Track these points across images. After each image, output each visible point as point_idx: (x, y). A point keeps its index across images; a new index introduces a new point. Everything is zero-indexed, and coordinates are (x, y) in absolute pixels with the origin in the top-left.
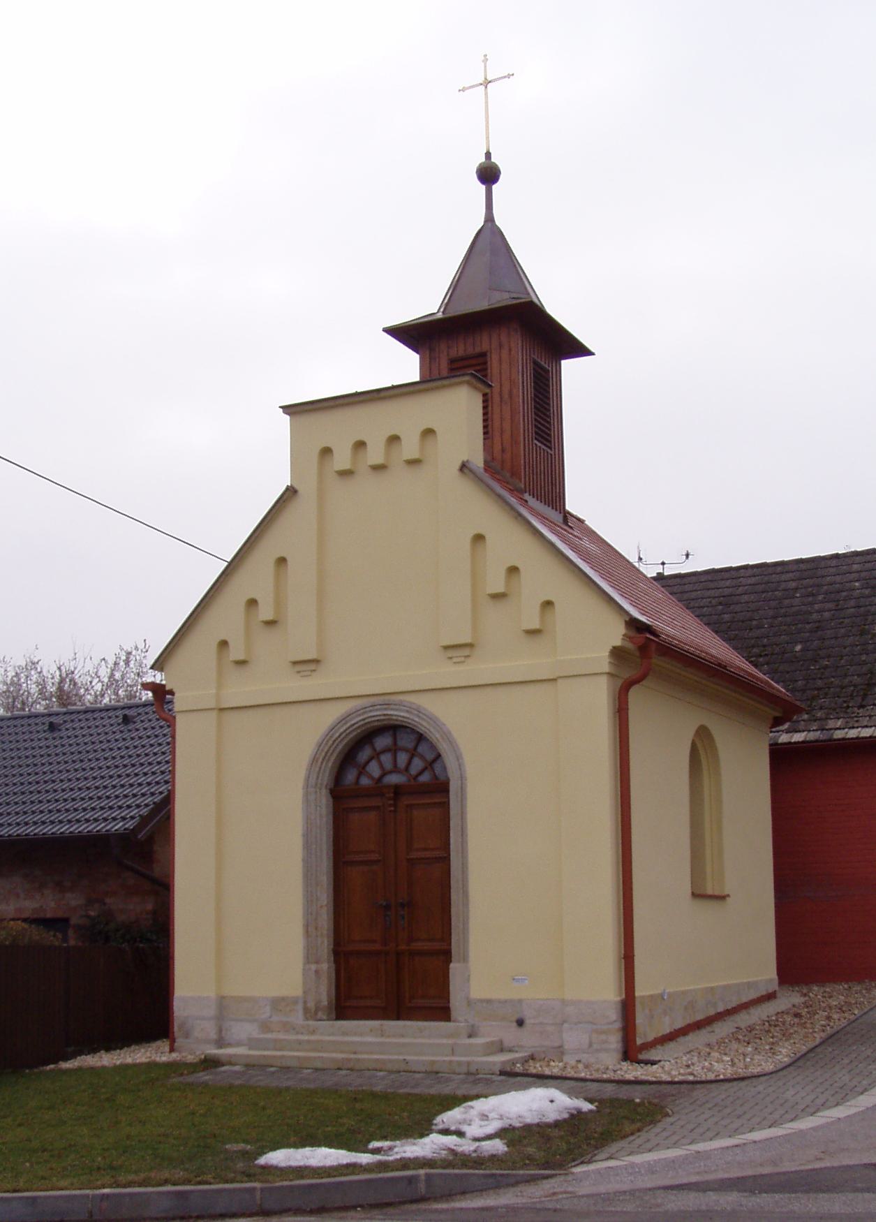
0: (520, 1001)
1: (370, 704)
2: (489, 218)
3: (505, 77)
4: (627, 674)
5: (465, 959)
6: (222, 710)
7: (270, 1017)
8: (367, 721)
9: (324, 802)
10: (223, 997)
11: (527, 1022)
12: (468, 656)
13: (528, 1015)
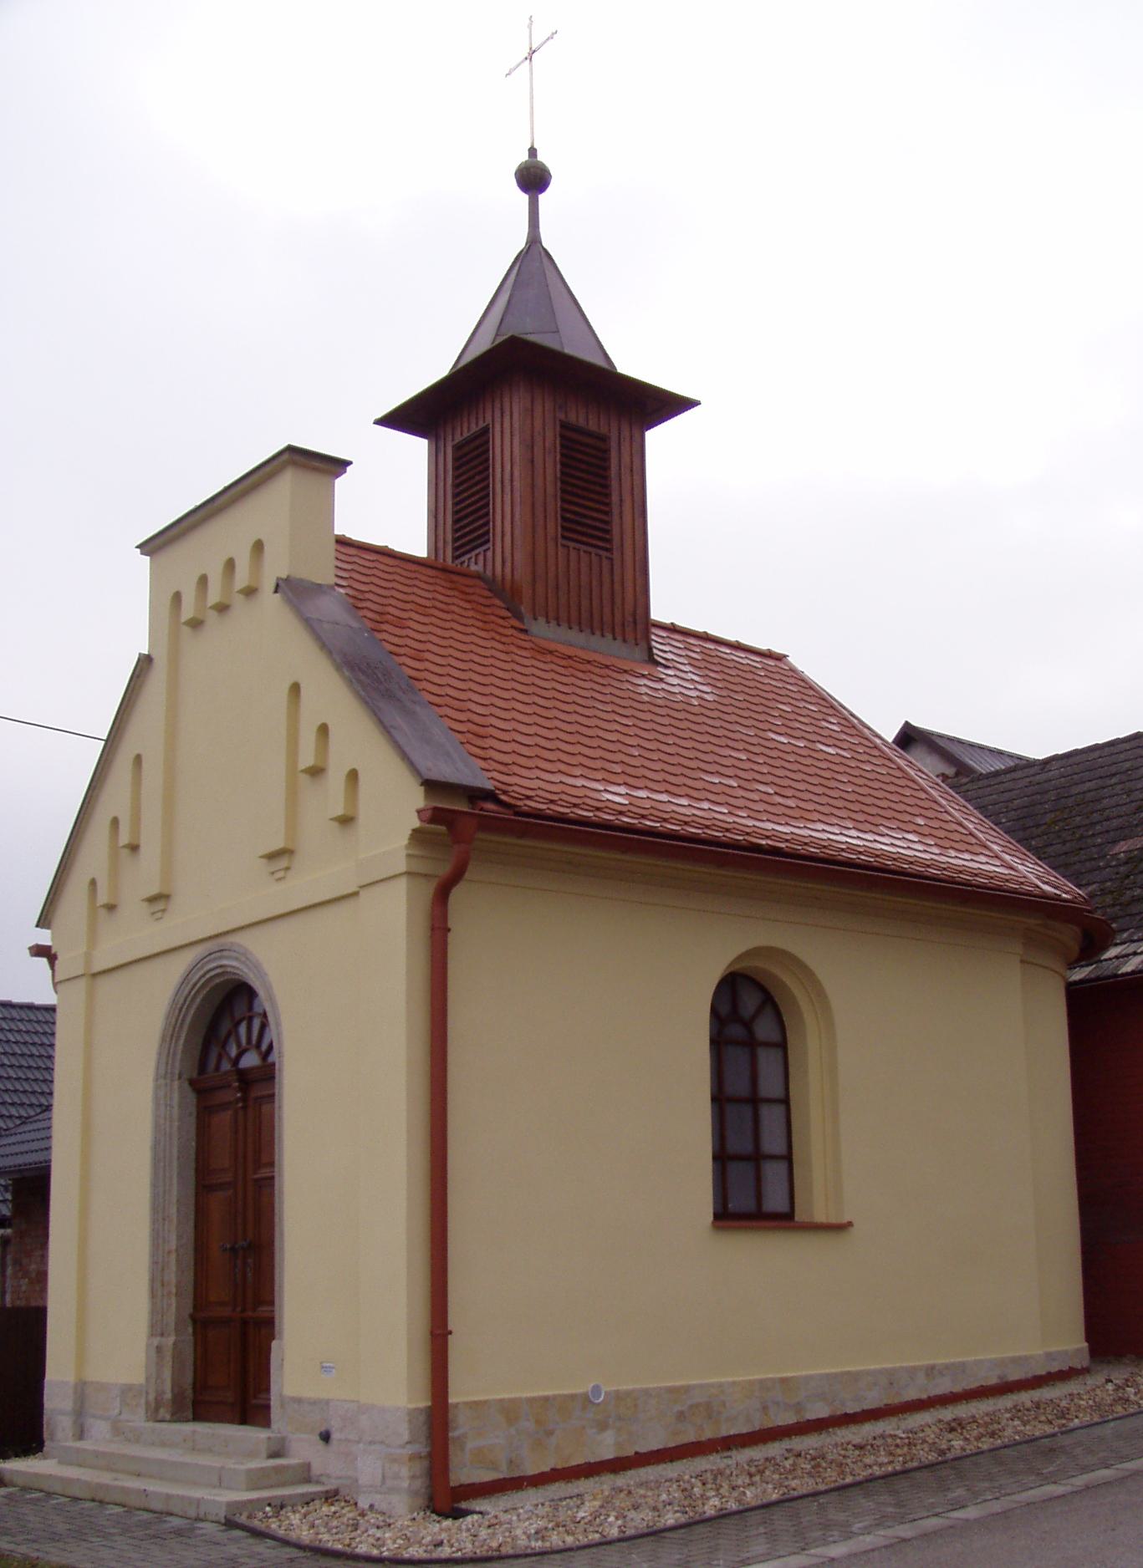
0: (327, 1402)
1: (207, 953)
2: (534, 239)
3: (548, 39)
4: (444, 869)
5: (281, 1339)
6: (95, 975)
7: (120, 1414)
8: (208, 976)
9: (180, 1097)
10: (85, 1383)
11: (335, 1436)
12: (287, 869)
13: (335, 1426)
